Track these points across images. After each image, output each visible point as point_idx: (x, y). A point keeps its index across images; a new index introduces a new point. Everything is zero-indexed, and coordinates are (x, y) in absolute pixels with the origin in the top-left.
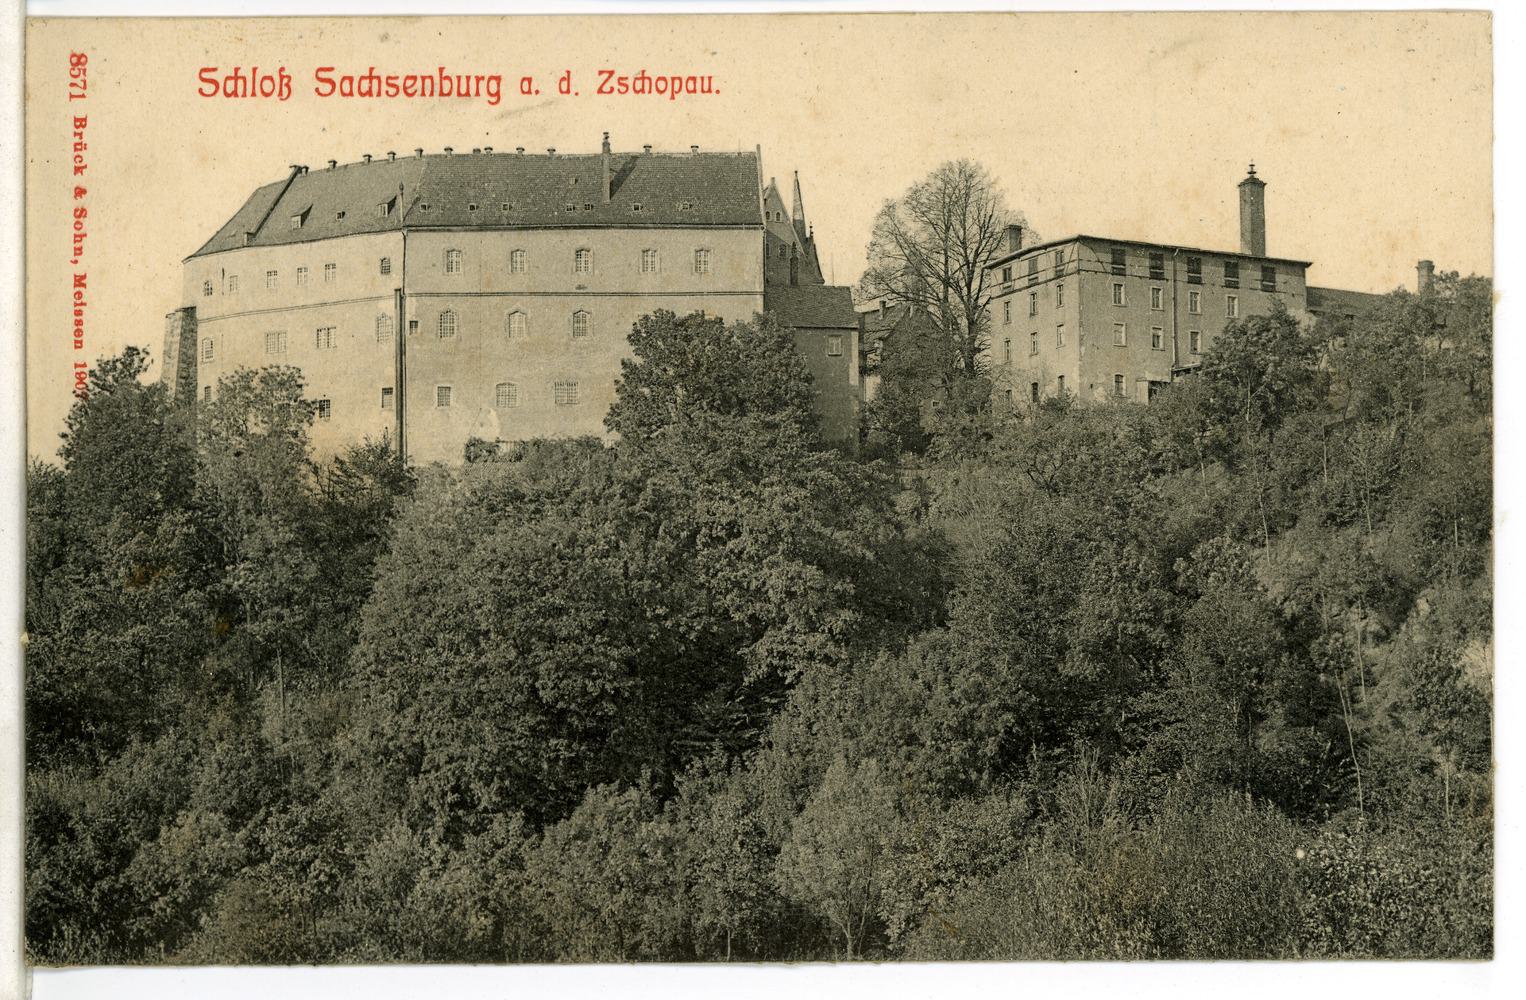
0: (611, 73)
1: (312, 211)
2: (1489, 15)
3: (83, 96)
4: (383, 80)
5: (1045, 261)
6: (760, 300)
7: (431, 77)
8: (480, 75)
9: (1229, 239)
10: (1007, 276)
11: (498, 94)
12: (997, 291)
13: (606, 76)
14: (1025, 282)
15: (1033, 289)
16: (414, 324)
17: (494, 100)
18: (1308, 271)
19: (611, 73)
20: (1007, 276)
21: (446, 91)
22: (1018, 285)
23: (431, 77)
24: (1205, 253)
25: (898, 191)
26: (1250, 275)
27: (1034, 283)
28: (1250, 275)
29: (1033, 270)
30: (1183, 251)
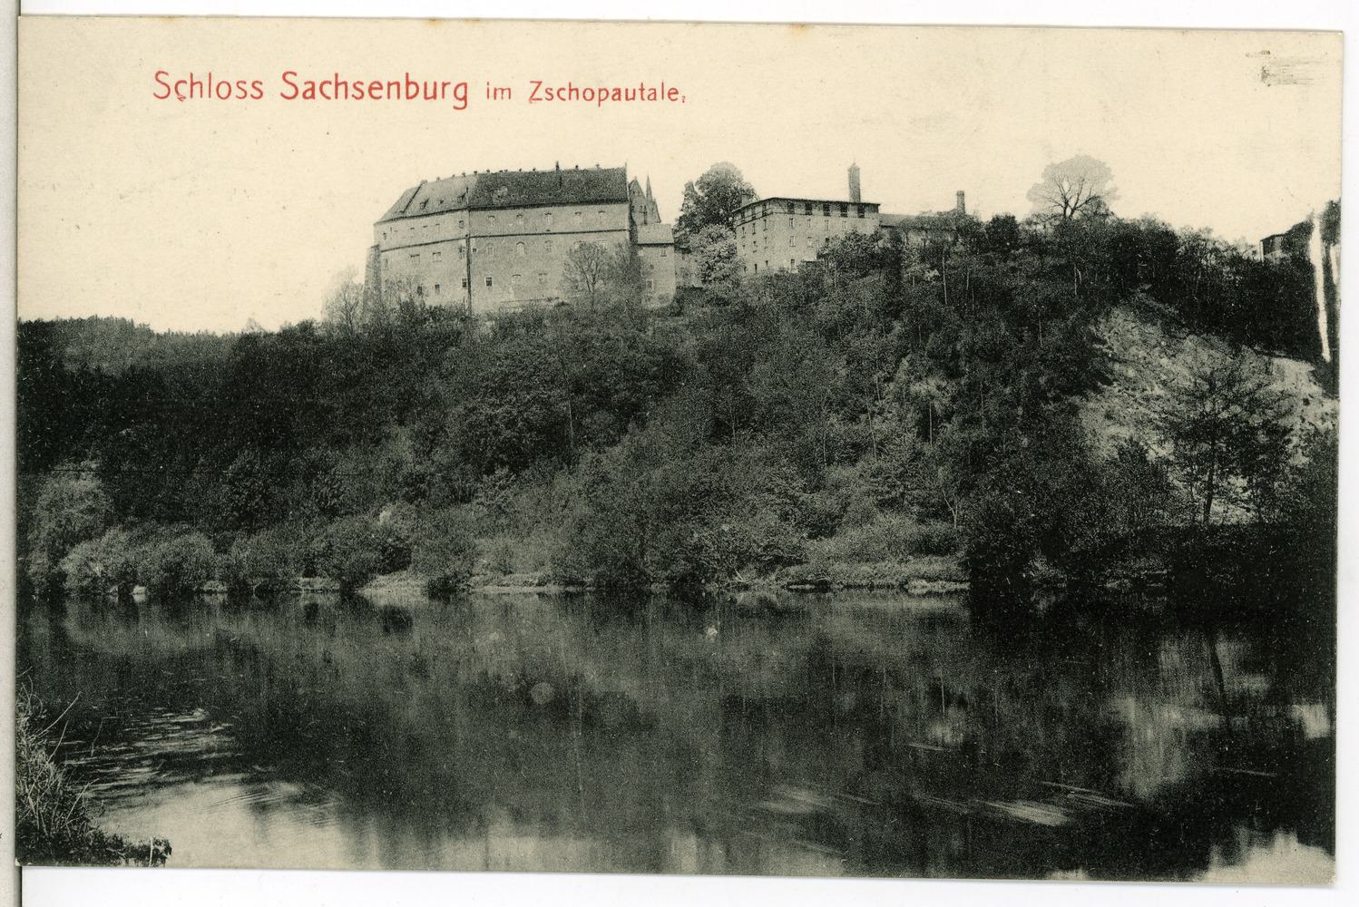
0: (540, 83)
1: (650, 178)
2: (1339, 33)
3: (509, 89)
4: (350, 86)
5: (759, 210)
6: (628, 233)
7: (398, 84)
8: (446, 81)
9: (845, 196)
10: (743, 217)
11: (465, 98)
12: (739, 223)
13: (536, 85)
14: (750, 218)
15: (754, 222)
16: (475, 250)
17: (461, 104)
18: (879, 207)
19: (540, 83)
20: (743, 217)
21: (411, 94)
22: (747, 219)
23: (398, 84)
24: (831, 202)
25: (695, 178)
26: (852, 212)
27: (754, 219)
28: (852, 212)
29: (754, 213)
30: (820, 202)
